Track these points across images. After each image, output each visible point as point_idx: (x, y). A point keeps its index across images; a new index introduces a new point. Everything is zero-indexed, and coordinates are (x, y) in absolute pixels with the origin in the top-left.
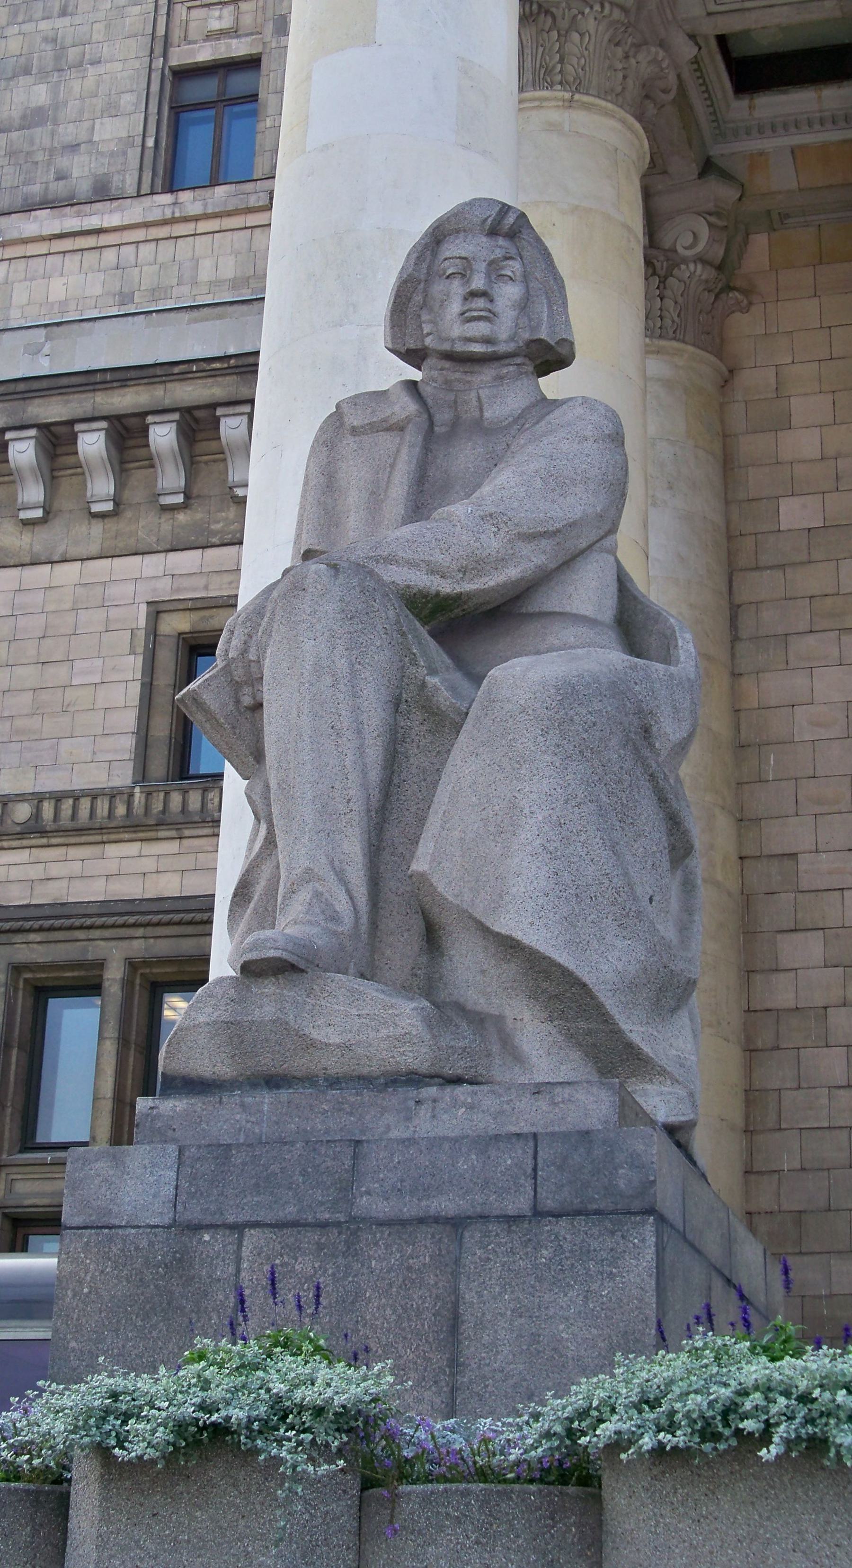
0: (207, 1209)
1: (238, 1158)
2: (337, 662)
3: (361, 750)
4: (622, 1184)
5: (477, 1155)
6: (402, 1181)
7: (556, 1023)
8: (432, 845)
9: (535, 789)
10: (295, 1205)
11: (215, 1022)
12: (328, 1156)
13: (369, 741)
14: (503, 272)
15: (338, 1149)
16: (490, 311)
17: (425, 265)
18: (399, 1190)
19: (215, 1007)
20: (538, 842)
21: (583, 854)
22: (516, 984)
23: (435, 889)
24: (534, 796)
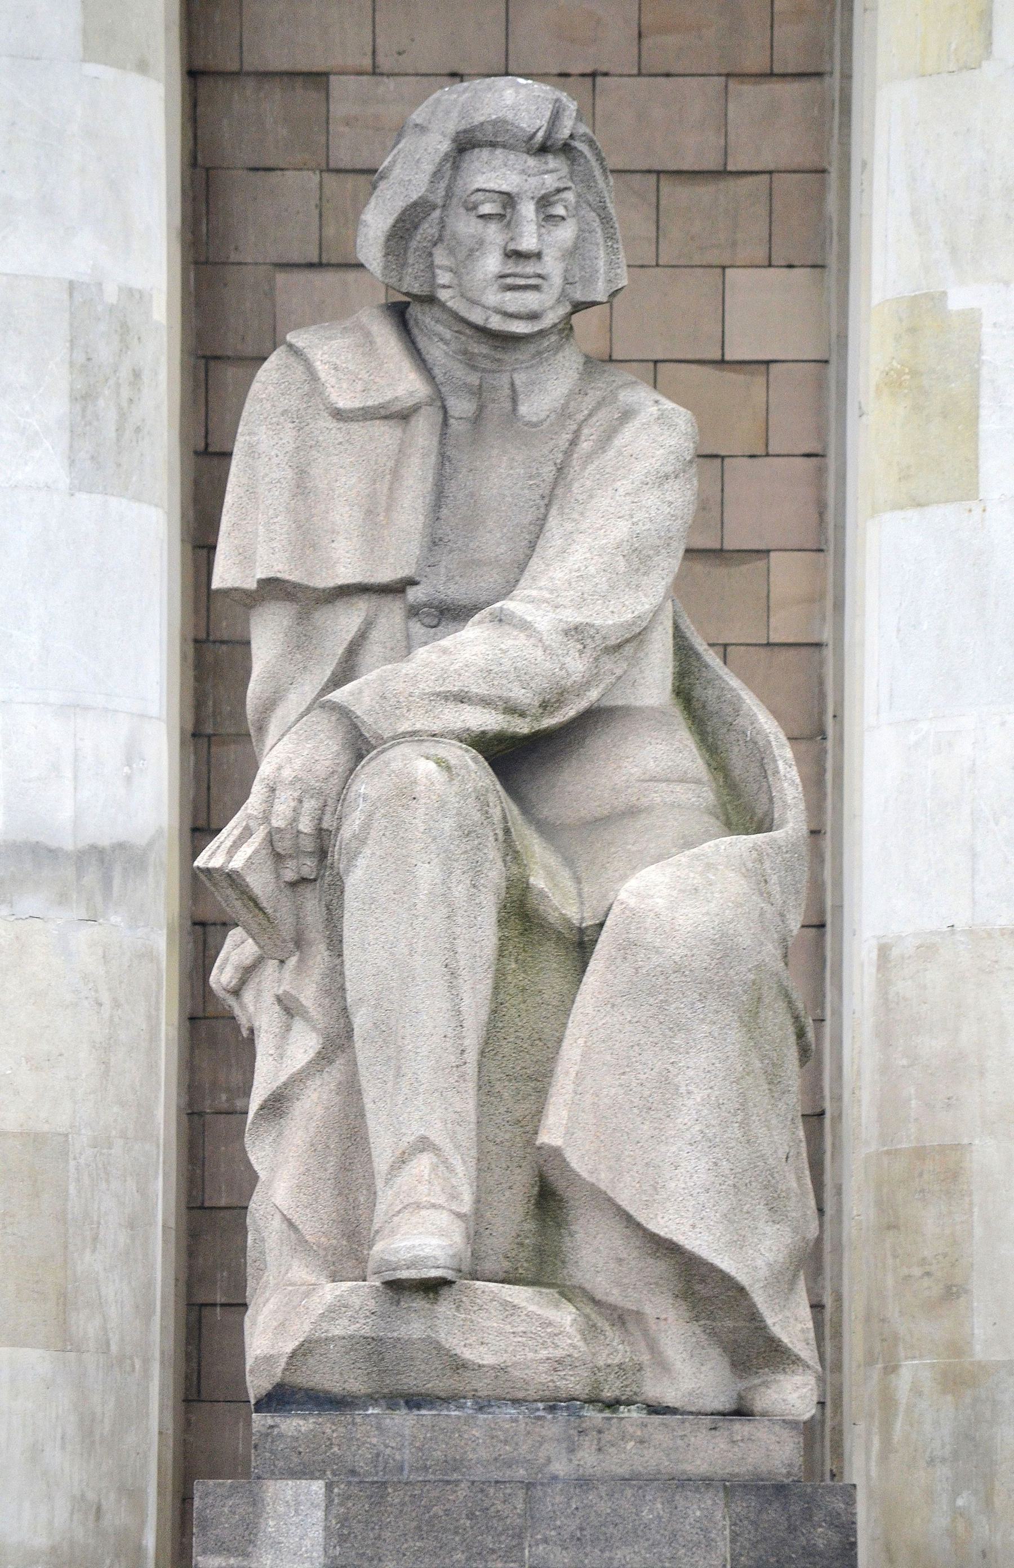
0: (364, 1554)
1: (394, 1497)
2: (454, 889)
4: (821, 1543)
5: (663, 1504)
6: (582, 1529)
7: (702, 1322)
8: (565, 1113)
9: (691, 1064)
10: (463, 1552)
11: (352, 1337)
12: (496, 1498)
15: (508, 1491)
16: (539, 276)
17: (443, 185)
18: (578, 1539)
19: (353, 1320)
20: (697, 1128)
22: (661, 1282)
23: (568, 1165)
24: (691, 1073)
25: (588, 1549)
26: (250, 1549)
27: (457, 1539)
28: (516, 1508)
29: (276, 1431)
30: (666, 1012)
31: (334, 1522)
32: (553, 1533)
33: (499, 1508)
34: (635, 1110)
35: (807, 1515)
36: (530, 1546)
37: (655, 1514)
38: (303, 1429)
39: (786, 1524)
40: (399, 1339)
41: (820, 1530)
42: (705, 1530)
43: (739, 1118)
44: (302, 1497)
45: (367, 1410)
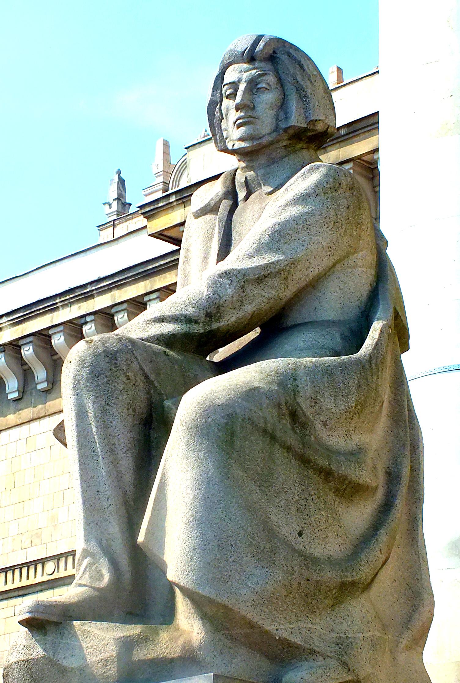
3: (115, 463)
13: (121, 455)
14: (259, 86)
21: (223, 516)
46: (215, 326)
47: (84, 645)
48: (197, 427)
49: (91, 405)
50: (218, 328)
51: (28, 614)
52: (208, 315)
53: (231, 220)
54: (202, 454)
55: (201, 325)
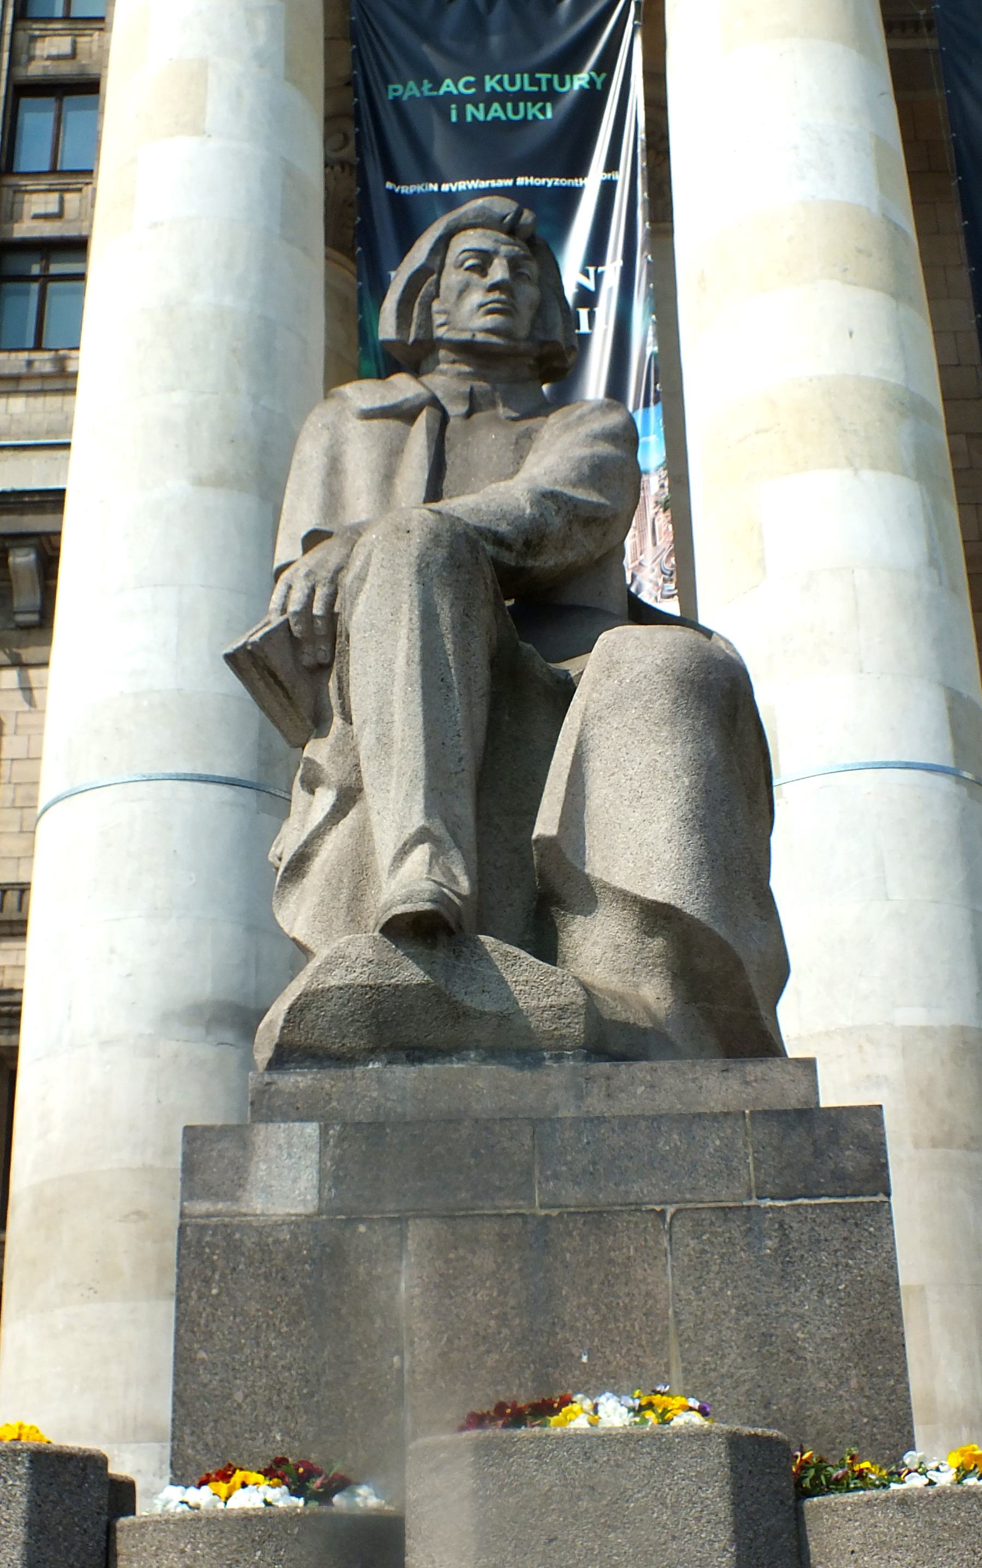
4: (850, 1166)
5: (680, 1134)
6: (594, 1163)
11: (349, 986)
14: (522, 270)
15: (515, 1128)
18: (591, 1173)
25: (602, 1183)
26: (238, 1194)
27: (461, 1178)
28: (523, 1145)
29: (273, 1088)
30: (651, 710)
31: (329, 1164)
32: (564, 1168)
33: (506, 1145)
34: (627, 803)
35: (833, 1139)
36: (539, 1183)
37: (672, 1145)
38: (301, 1085)
39: (812, 1149)
40: (398, 986)
41: (848, 1153)
42: (727, 1160)
43: (726, 808)
44: (295, 1140)
45: (368, 1065)
46: (530, 563)
47: (509, 978)
48: (692, 682)
49: (446, 607)
50: (532, 568)
51: (429, 904)
52: (527, 544)
53: (444, 436)
54: (699, 724)
55: (514, 554)
